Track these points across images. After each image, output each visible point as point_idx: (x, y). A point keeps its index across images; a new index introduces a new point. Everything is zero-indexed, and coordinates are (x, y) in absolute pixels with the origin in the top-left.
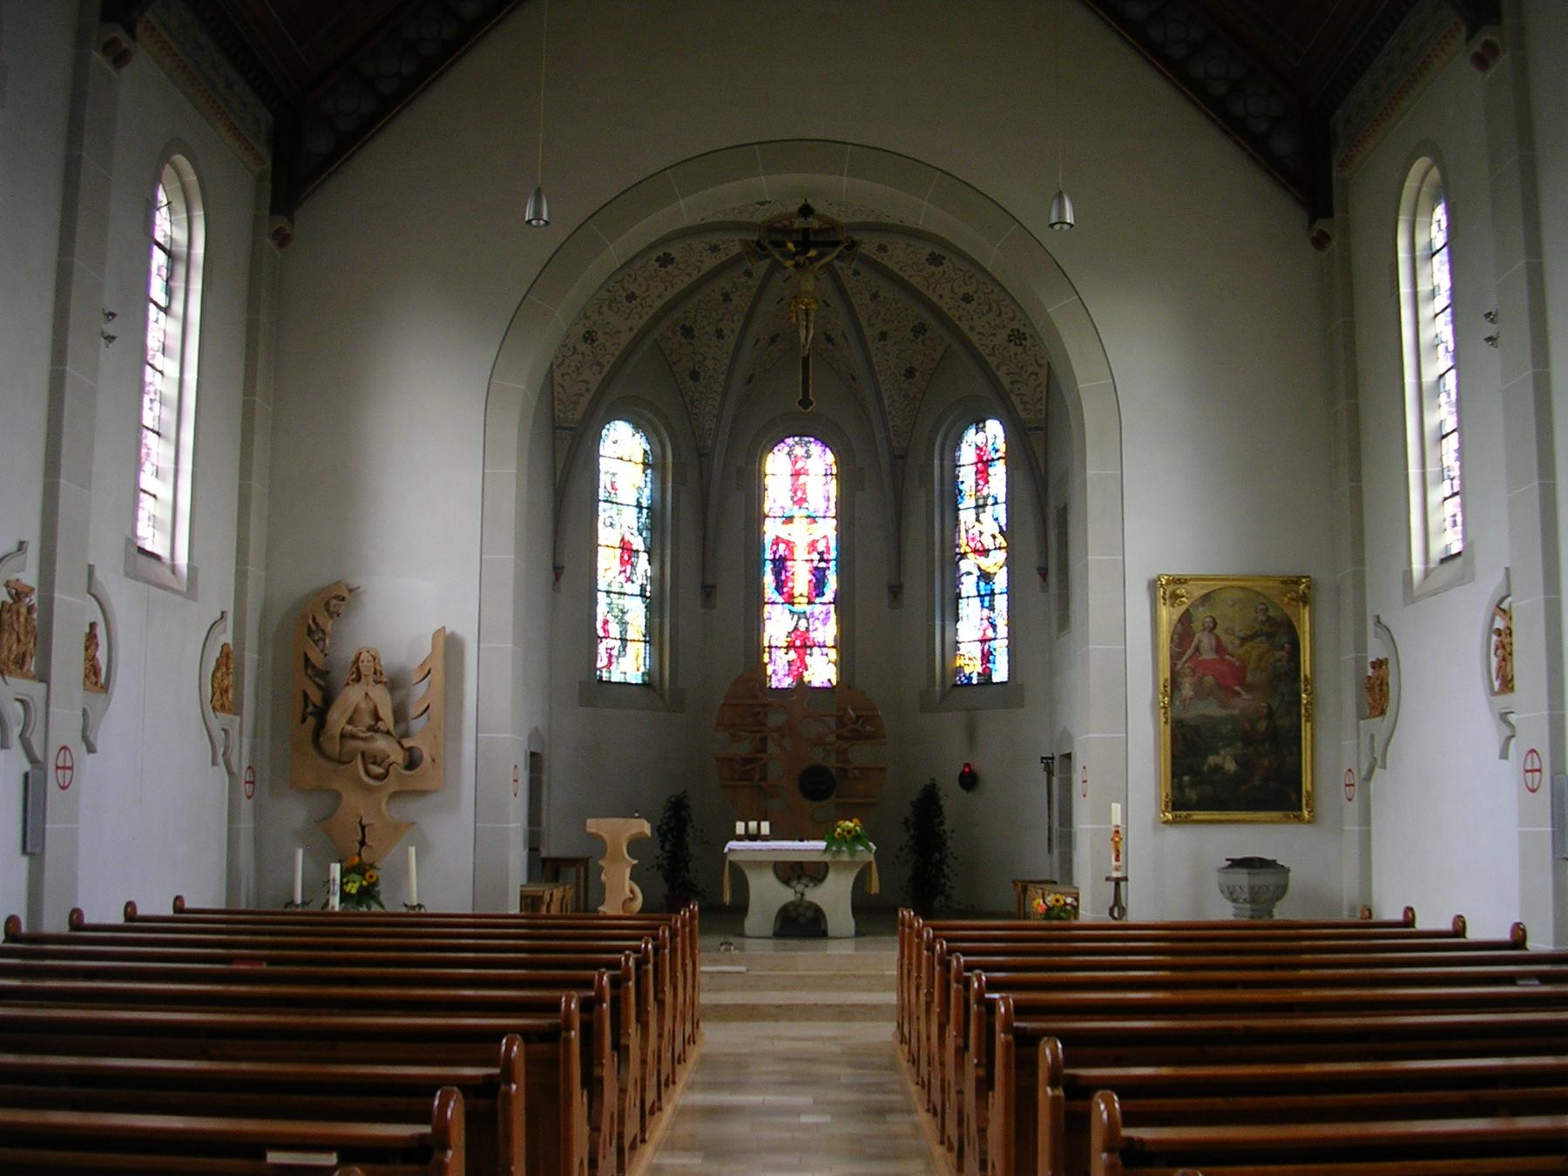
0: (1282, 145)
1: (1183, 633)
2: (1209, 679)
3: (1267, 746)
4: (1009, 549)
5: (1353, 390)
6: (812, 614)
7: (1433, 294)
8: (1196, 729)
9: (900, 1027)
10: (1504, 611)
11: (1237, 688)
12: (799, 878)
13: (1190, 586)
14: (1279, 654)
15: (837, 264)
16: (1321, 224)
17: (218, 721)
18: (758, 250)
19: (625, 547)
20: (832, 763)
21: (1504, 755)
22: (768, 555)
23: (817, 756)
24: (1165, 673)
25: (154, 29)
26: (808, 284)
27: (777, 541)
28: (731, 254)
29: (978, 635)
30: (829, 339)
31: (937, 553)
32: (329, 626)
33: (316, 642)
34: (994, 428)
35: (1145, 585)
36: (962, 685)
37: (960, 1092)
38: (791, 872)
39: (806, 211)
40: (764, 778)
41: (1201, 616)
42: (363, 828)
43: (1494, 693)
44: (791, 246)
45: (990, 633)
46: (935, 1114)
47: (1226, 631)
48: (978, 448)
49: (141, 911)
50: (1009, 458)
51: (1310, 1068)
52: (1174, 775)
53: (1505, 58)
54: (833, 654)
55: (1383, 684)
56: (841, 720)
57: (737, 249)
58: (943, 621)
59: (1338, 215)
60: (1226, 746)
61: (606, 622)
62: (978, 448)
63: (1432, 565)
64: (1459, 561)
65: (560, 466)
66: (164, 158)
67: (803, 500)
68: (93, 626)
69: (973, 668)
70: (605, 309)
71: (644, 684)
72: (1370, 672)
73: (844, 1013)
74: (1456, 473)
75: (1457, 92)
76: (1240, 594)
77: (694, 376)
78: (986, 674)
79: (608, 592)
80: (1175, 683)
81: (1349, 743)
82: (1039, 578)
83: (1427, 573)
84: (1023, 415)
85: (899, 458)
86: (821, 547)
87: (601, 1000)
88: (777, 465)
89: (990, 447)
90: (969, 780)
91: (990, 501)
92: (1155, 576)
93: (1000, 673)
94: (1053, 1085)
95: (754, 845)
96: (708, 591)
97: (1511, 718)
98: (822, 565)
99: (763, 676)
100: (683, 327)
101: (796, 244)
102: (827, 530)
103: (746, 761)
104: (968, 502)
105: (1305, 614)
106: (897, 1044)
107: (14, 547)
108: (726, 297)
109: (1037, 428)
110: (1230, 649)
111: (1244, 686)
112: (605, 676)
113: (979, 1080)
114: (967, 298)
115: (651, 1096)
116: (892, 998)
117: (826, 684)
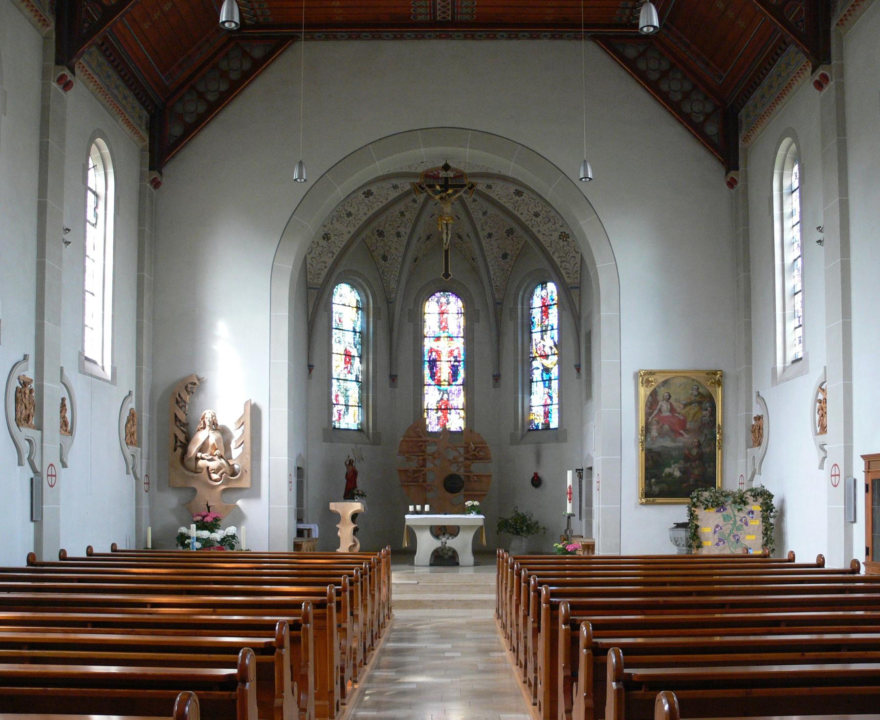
0: (712, 129)
1: (652, 402)
2: (666, 427)
3: (697, 462)
4: (560, 355)
5: (747, 267)
6: (451, 391)
7: (792, 214)
8: (659, 454)
9: (498, 610)
10: (823, 390)
11: (681, 432)
12: (444, 534)
13: (657, 377)
14: (704, 413)
15: (464, 196)
16: (732, 174)
17: (129, 450)
18: (419, 188)
19: (348, 355)
20: (461, 472)
21: (821, 467)
22: (426, 358)
23: (453, 469)
24: (642, 423)
25: (83, 67)
26: (448, 209)
27: (431, 351)
28: (405, 190)
29: (542, 402)
30: (460, 237)
31: (520, 357)
32: (187, 398)
33: (181, 408)
34: (551, 287)
35: (632, 376)
36: (533, 430)
37: (526, 637)
38: (438, 531)
39: (446, 167)
40: (424, 481)
41: (662, 392)
42: (209, 508)
43: (816, 434)
44: (438, 188)
45: (549, 402)
46: (514, 651)
47: (676, 400)
48: (542, 298)
49: (95, 551)
50: (559, 304)
51: (776, 668)
52: (646, 478)
53: (832, 83)
54: (462, 413)
55: (760, 428)
56: (467, 449)
57: (408, 187)
58: (523, 394)
59: (741, 168)
60: (674, 463)
61: (337, 396)
62: (542, 298)
63: (787, 365)
64: (801, 362)
65: (311, 310)
66: (92, 141)
67: (446, 327)
68: (63, 400)
69: (539, 421)
70: (335, 221)
71: (358, 430)
72: (753, 422)
73: (467, 604)
74: (800, 314)
75: (805, 103)
76: (683, 380)
77: (385, 258)
78: (547, 426)
79: (338, 379)
80: (647, 429)
81: (741, 461)
82: (575, 371)
83: (784, 369)
84: (568, 280)
85: (498, 305)
86: (456, 353)
87: (345, 591)
88: (431, 307)
89: (549, 298)
90: (537, 481)
91: (549, 328)
92: (637, 370)
93: (554, 424)
94: (565, 624)
95: (418, 517)
96: (393, 378)
97: (825, 447)
98: (456, 363)
99: (426, 426)
100: (378, 231)
101: (441, 186)
102: (459, 344)
103: (415, 472)
104: (536, 329)
105: (719, 390)
106: (495, 619)
107: (22, 358)
108: (402, 214)
109: (575, 288)
110: (678, 410)
111: (686, 431)
112: (337, 426)
113: (534, 629)
114: (536, 215)
115: (368, 643)
116: (494, 597)
117: (459, 430)
